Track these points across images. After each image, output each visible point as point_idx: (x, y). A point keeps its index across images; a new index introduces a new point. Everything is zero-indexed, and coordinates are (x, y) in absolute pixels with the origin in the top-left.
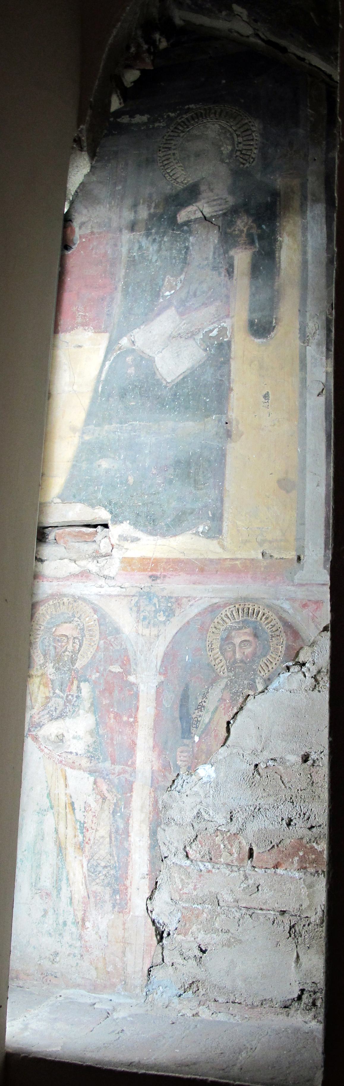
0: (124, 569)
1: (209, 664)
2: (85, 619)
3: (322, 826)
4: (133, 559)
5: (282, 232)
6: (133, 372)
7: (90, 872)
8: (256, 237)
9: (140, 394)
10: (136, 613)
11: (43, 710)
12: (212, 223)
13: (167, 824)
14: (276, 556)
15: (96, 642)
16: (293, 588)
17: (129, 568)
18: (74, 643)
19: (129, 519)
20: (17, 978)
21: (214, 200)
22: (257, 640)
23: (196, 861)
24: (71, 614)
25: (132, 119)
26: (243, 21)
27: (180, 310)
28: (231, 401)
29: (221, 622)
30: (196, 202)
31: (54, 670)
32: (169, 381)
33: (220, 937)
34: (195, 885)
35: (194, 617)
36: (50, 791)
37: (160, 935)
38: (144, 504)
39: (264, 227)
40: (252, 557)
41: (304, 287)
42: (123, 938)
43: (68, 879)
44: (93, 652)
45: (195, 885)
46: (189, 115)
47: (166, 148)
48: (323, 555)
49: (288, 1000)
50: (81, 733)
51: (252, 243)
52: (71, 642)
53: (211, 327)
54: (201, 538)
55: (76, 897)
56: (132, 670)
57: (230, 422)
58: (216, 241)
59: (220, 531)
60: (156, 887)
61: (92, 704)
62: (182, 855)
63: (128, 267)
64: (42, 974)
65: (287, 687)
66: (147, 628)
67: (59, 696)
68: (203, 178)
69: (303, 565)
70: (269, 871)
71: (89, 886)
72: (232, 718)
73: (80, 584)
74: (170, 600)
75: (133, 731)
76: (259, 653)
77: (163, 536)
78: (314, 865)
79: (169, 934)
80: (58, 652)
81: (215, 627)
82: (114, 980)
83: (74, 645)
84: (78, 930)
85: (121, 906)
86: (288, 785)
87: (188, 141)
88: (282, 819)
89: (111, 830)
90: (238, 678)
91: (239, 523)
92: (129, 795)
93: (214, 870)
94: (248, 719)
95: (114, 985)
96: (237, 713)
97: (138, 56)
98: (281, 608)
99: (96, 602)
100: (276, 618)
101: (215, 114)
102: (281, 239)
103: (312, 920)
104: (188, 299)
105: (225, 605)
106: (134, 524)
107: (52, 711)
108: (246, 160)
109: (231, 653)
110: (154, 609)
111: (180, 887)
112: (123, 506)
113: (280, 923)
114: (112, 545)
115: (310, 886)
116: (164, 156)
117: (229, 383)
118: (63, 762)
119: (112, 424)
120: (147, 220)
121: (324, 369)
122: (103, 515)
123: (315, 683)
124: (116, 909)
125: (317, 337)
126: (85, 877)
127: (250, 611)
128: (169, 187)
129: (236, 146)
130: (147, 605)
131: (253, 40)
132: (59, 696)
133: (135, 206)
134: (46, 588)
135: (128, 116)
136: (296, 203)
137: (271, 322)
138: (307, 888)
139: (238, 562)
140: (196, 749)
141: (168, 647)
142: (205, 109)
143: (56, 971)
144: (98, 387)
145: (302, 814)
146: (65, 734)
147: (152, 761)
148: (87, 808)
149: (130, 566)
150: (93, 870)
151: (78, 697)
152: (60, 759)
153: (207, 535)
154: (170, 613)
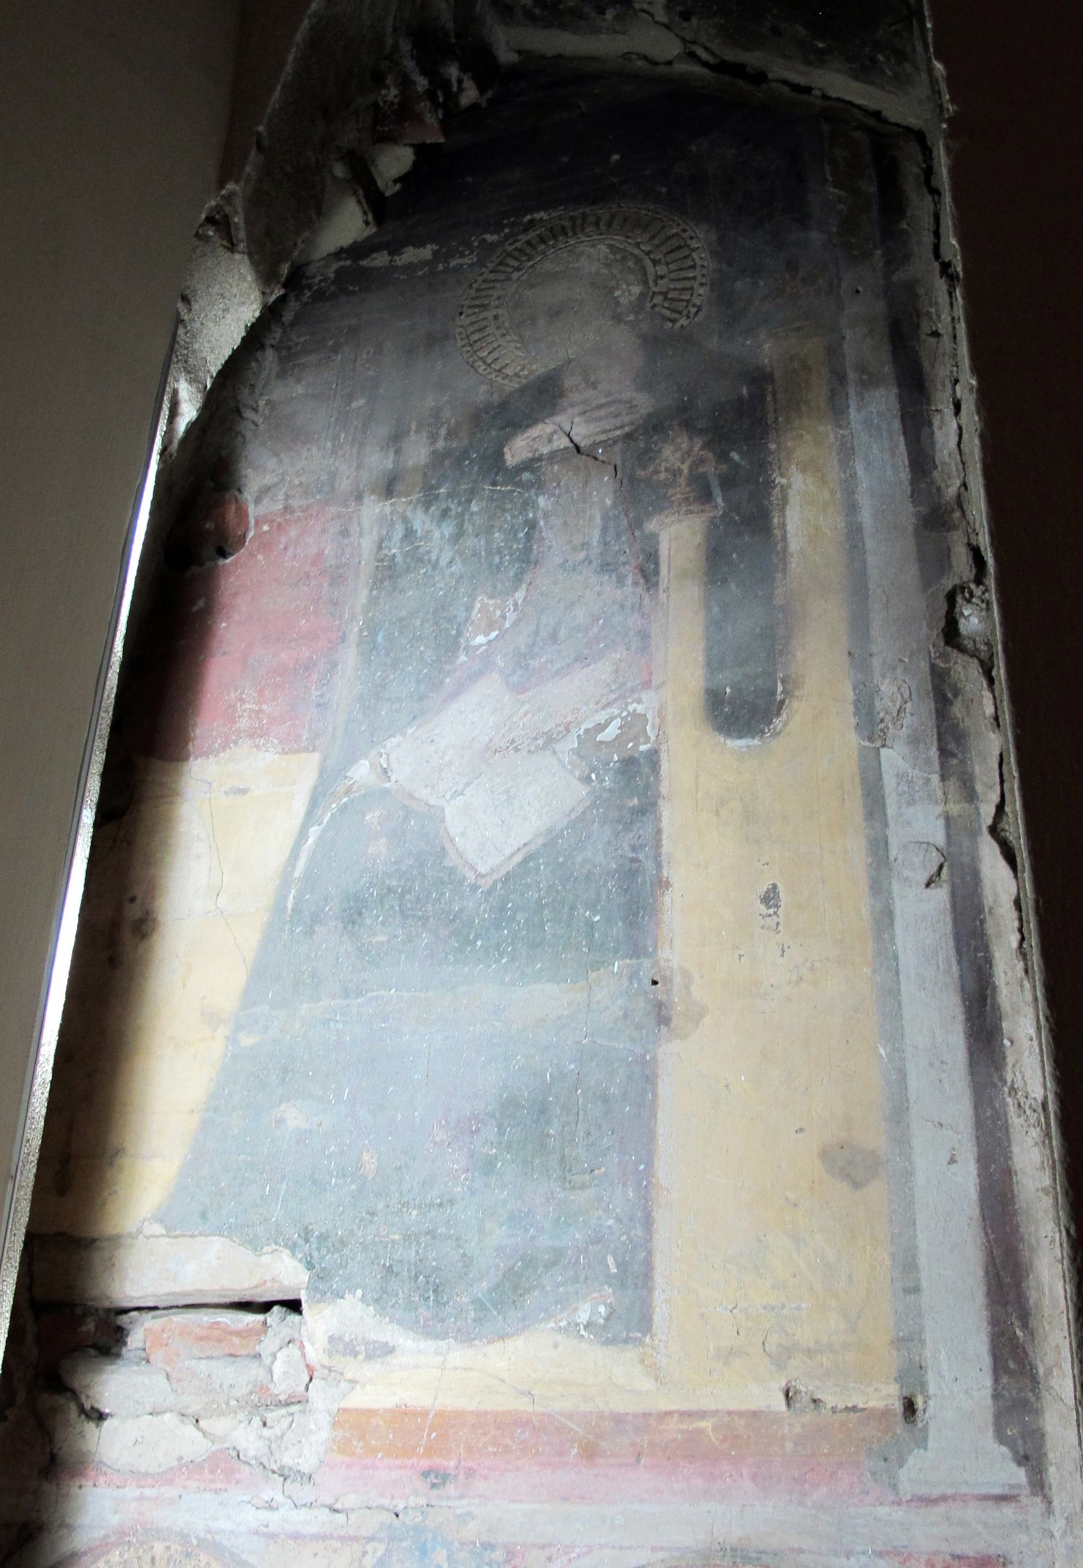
0: (343, 1447)
4: (371, 1413)
5: (785, 463)
6: (384, 851)
8: (715, 483)
9: (401, 911)
12: (596, 459)
14: (830, 1399)
16: (898, 1514)
19: (364, 1287)
21: (600, 407)
25: (396, 258)
26: (657, 23)
27: (515, 678)
28: (666, 918)
30: (553, 414)
32: (482, 870)
38: (406, 1238)
39: (735, 456)
40: (753, 1407)
41: (858, 589)
46: (532, 235)
47: (477, 306)
48: (988, 1392)
51: (705, 496)
53: (602, 717)
54: (584, 1346)
57: (664, 978)
58: (608, 502)
59: (645, 1322)
63: (377, 583)
68: (570, 361)
69: (925, 1428)
73: (208, 1496)
77: (467, 1338)
87: (531, 286)
97: (405, 112)
101: (597, 224)
102: (784, 481)
104: (536, 650)
108: (680, 313)
112: (343, 1243)
114: (310, 1369)
116: (472, 323)
117: (659, 866)
119: (320, 1000)
120: (426, 466)
121: (939, 809)
122: (286, 1274)
125: (907, 720)
128: (483, 388)
129: (651, 283)
131: (681, 67)
133: (397, 438)
135: (385, 252)
136: (819, 392)
137: (774, 693)
139: (706, 1424)
142: (572, 218)
144: (286, 898)
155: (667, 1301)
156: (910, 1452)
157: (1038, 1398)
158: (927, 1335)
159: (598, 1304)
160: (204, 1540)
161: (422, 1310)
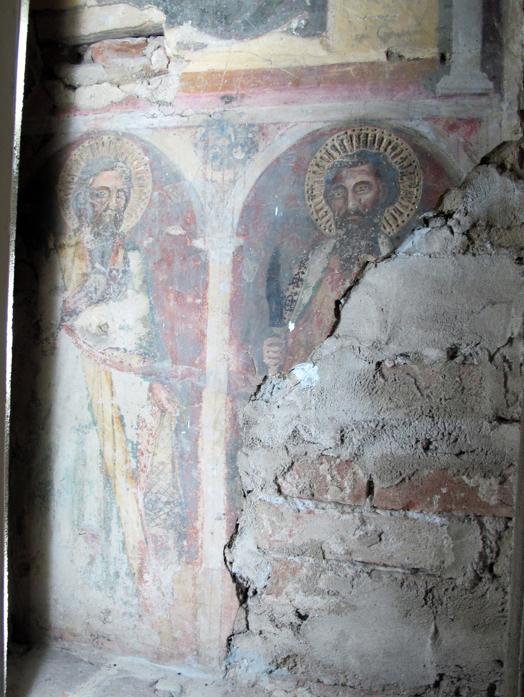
0: (185, 89)
1: (308, 219)
2: (132, 164)
3: (476, 452)
4: (197, 74)
7: (148, 509)
10: (202, 151)
11: (79, 292)
13: (251, 447)
14: (407, 55)
15: (148, 195)
16: (434, 102)
17: (192, 88)
18: (118, 197)
19: (192, 19)
20: (61, 638)
22: (379, 181)
23: (292, 497)
24: (113, 157)
29: (326, 157)
31: (92, 237)
33: (325, 601)
34: (291, 531)
35: (286, 152)
36: (91, 402)
37: (243, 593)
42: (194, 596)
43: (119, 518)
44: (145, 208)
45: (291, 531)
48: (479, 50)
49: (421, 687)
50: (130, 321)
52: (114, 196)
54: (295, 38)
55: (131, 541)
56: (199, 232)
60: (237, 531)
61: (144, 281)
62: (272, 489)
64: (92, 635)
65: (424, 250)
66: (219, 170)
67: (100, 273)
69: (450, 67)
70: (396, 514)
71: (146, 528)
72: (344, 296)
73: (126, 115)
74: (251, 129)
75: (201, 317)
76: (383, 200)
77: (240, 38)
78: (464, 507)
79: (255, 593)
80: (97, 212)
81: (317, 165)
82: (183, 649)
83: (119, 200)
84: (134, 583)
85: (190, 555)
86: (425, 392)
88: (417, 441)
89: (173, 453)
90: (352, 238)
91: (350, 11)
92: (197, 406)
93: (316, 511)
94: (367, 296)
95: (182, 655)
96: (350, 289)
98: (416, 132)
99: (147, 139)
100: (408, 147)
103: (459, 582)
105: (332, 131)
106: (198, 25)
107: (91, 292)
109: (342, 201)
110: (227, 143)
111: (270, 532)
113: (412, 585)
115: (456, 536)
118: (108, 362)
122: (155, 16)
123: (467, 242)
124: (184, 559)
126: (141, 515)
127: (369, 138)
130: (218, 138)
132: (100, 273)
134: (80, 124)
138: (453, 540)
139: (350, 69)
140: (291, 341)
141: (248, 196)
143: (109, 633)
145: (446, 433)
146: (109, 324)
147: (229, 359)
148: (141, 424)
149: (193, 85)
150: (151, 507)
151: (125, 272)
152: (104, 357)
153: (306, 32)
154: (251, 147)
155: (333, 16)
156: (442, 76)
157: (502, 53)
158: (454, 26)
159: (301, 20)
160: (125, 133)
161: (219, 28)
